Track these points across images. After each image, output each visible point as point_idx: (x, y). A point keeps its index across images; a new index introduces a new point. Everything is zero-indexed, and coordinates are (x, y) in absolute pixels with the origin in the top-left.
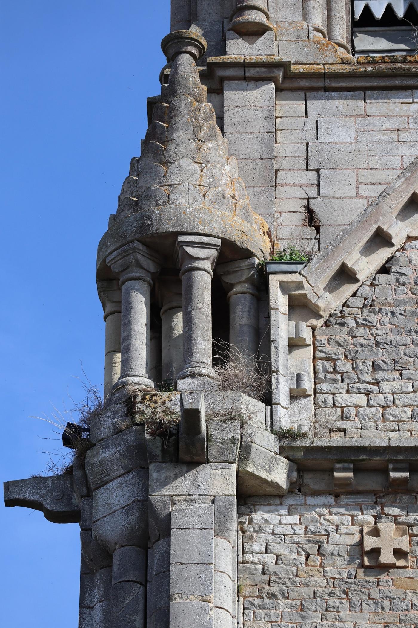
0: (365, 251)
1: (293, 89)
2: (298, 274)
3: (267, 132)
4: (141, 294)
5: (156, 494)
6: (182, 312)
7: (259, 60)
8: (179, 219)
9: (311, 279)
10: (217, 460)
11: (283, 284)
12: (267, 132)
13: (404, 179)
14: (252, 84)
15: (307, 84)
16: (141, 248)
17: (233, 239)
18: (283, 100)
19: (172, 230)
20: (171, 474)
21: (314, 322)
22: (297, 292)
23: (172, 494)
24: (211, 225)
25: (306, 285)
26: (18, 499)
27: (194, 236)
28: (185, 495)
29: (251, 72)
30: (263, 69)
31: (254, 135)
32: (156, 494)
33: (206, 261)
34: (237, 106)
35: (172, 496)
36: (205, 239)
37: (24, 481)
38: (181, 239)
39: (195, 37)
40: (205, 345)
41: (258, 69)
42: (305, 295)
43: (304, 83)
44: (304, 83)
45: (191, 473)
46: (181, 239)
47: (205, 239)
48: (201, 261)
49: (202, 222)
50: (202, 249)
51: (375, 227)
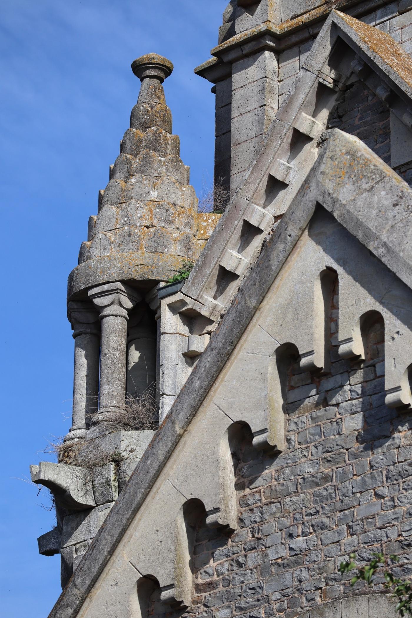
0: (244, 244)
1: (290, 47)
2: (179, 293)
3: (260, 107)
4: (82, 348)
5: (66, 545)
6: (134, 345)
7: (245, 37)
8: (87, 275)
9: (191, 292)
10: (101, 503)
11: (171, 305)
12: (260, 107)
13: (251, 169)
14: (251, 59)
15: (297, 39)
16: (75, 307)
17: (130, 277)
18: (291, 59)
19: (83, 287)
20: (74, 525)
21: (209, 328)
22: (184, 309)
23: (74, 543)
24: (109, 272)
25: (188, 300)
26: (47, 550)
27: (97, 288)
28: (82, 542)
29: (247, 49)
30: (253, 43)
31: (252, 113)
32: (66, 545)
33: (112, 306)
34: (241, 87)
35: (74, 545)
36: (106, 287)
37: (48, 534)
38: (91, 292)
39: (147, 62)
40: (109, 389)
41: (250, 45)
42: (191, 309)
43: (294, 39)
44: (294, 39)
45: (86, 520)
46: (91, 292)
47: (106, 287)
48: (107, 308)
49: (104, 271)
50: (106, 297)
51: (241, 223)
